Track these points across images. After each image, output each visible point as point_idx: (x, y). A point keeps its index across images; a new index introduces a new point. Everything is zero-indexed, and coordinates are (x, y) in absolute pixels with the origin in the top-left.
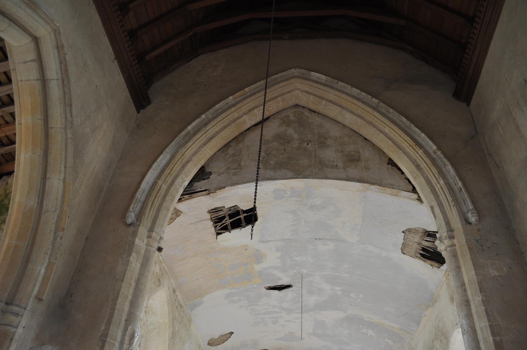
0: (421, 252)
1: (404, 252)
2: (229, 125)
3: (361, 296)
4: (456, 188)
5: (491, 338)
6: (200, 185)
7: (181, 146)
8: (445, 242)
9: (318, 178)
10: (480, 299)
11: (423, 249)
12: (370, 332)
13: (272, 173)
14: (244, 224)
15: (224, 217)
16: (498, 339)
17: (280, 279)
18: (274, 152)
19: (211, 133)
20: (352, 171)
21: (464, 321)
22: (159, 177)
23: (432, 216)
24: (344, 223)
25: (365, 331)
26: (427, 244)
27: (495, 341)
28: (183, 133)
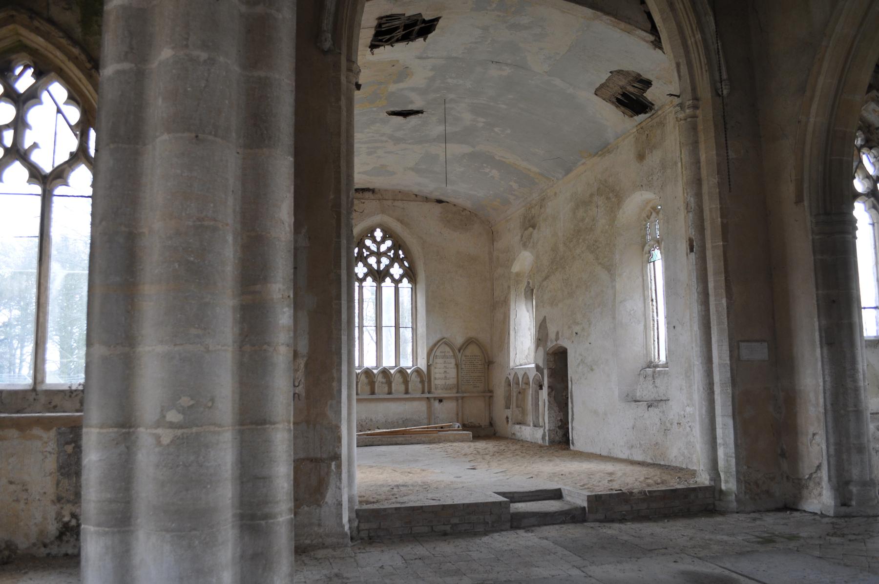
0: (620, 97)
1: (598, 93)
3: (509, 131)
5: (719, 219)
8: (688, 111)
10: (716, 181)
11: (624, 95)
12: (495, 173)
15: (396, 29)
16: (725, 221)
17: (412, 102)
21: (692, 199)
23: (676, 74)
24: (541, 49)
25: (487, 170)
26: (631, 89)
27: (722, 223)
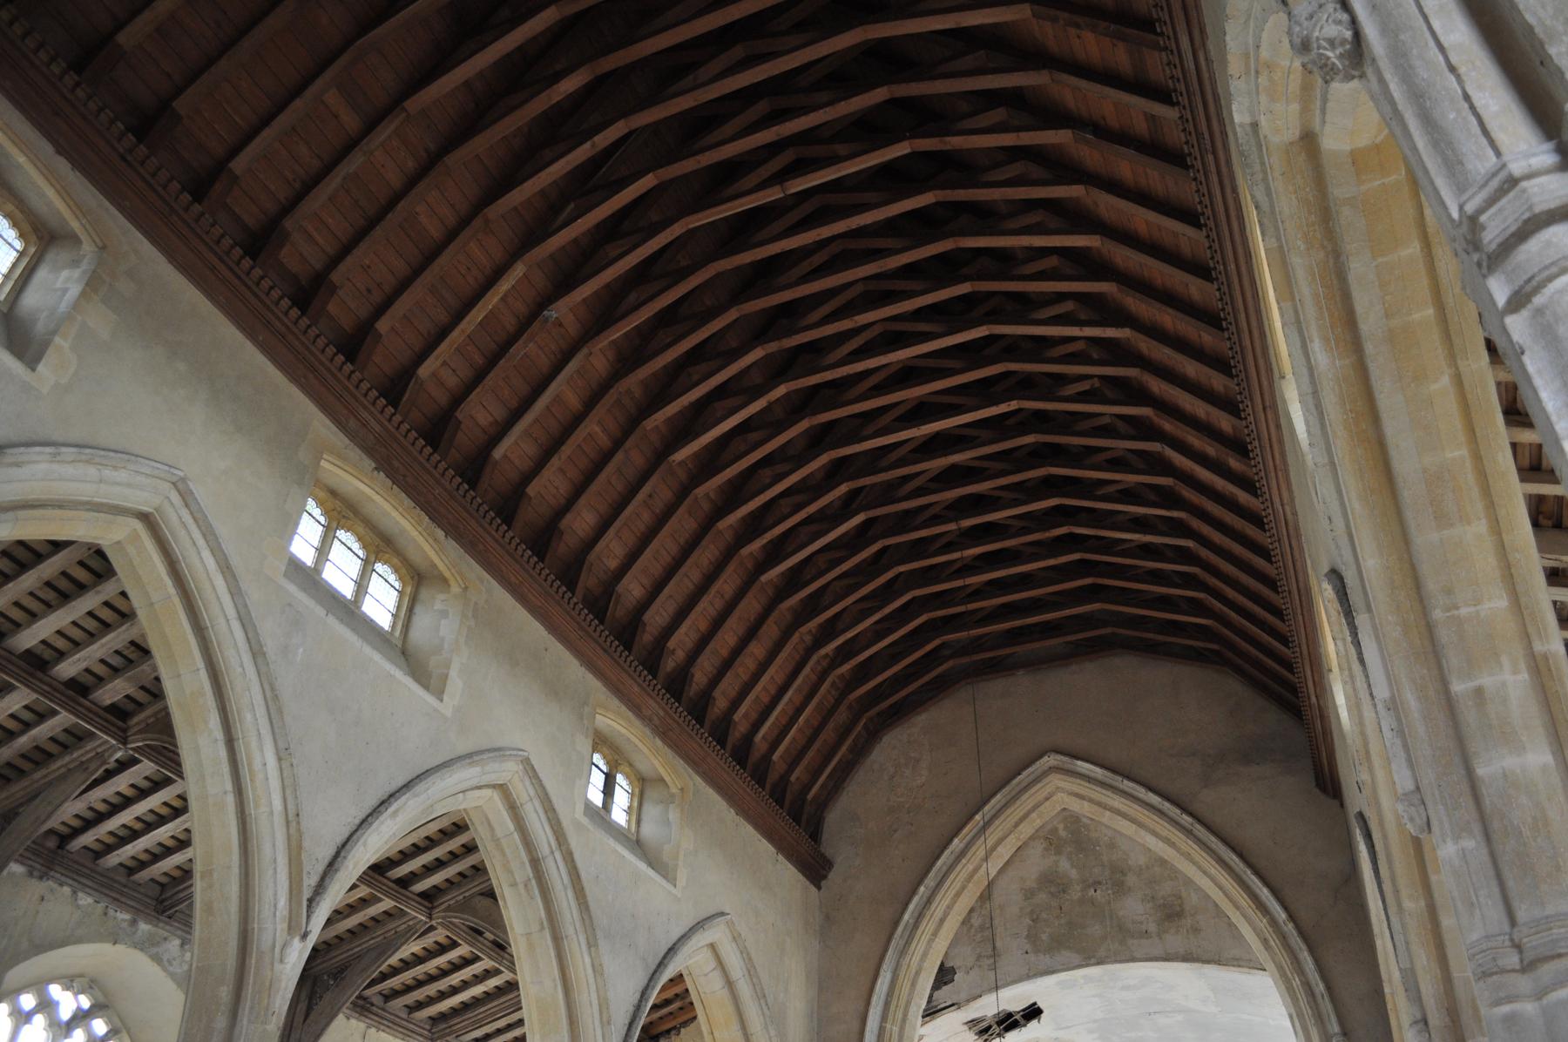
2: (963, 888)
4: (1317, 992)
6: (944, 995)
7: (903, 952)
9: (1121, 962)
13: (1045, 960)
14: (1022, 1022)
18: (1044, 915)
19: (939, 914)
20: (1175, 941)
22: (884, 1018)
28: (900, 929)
